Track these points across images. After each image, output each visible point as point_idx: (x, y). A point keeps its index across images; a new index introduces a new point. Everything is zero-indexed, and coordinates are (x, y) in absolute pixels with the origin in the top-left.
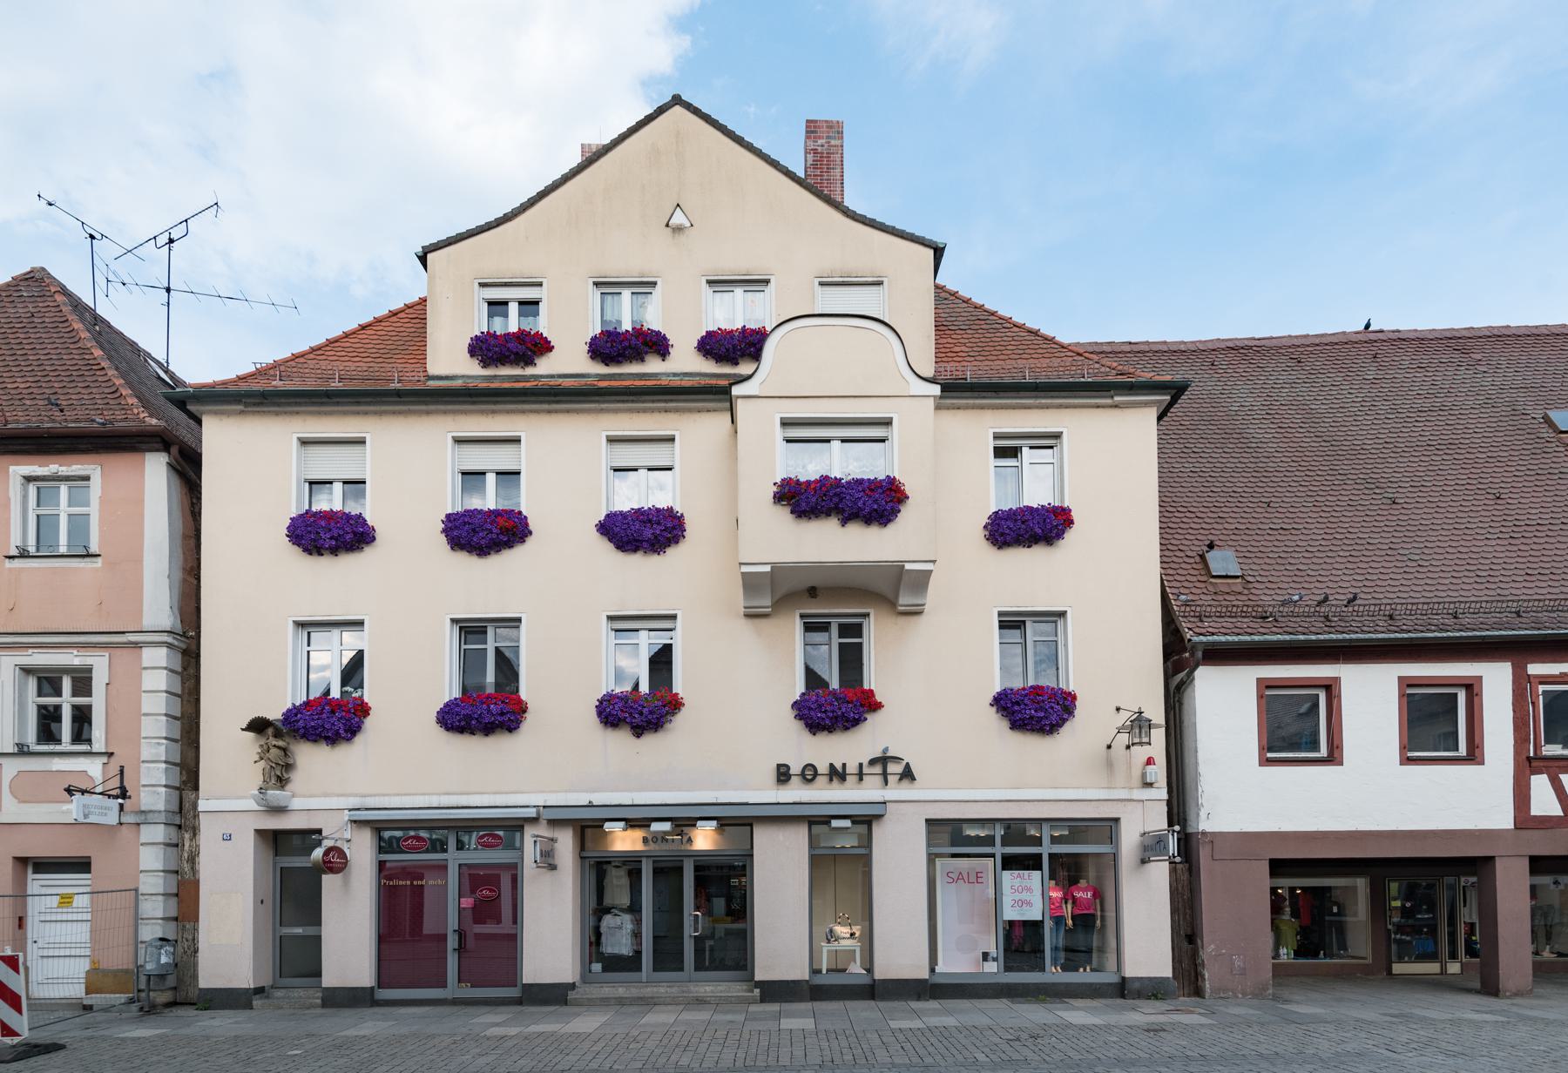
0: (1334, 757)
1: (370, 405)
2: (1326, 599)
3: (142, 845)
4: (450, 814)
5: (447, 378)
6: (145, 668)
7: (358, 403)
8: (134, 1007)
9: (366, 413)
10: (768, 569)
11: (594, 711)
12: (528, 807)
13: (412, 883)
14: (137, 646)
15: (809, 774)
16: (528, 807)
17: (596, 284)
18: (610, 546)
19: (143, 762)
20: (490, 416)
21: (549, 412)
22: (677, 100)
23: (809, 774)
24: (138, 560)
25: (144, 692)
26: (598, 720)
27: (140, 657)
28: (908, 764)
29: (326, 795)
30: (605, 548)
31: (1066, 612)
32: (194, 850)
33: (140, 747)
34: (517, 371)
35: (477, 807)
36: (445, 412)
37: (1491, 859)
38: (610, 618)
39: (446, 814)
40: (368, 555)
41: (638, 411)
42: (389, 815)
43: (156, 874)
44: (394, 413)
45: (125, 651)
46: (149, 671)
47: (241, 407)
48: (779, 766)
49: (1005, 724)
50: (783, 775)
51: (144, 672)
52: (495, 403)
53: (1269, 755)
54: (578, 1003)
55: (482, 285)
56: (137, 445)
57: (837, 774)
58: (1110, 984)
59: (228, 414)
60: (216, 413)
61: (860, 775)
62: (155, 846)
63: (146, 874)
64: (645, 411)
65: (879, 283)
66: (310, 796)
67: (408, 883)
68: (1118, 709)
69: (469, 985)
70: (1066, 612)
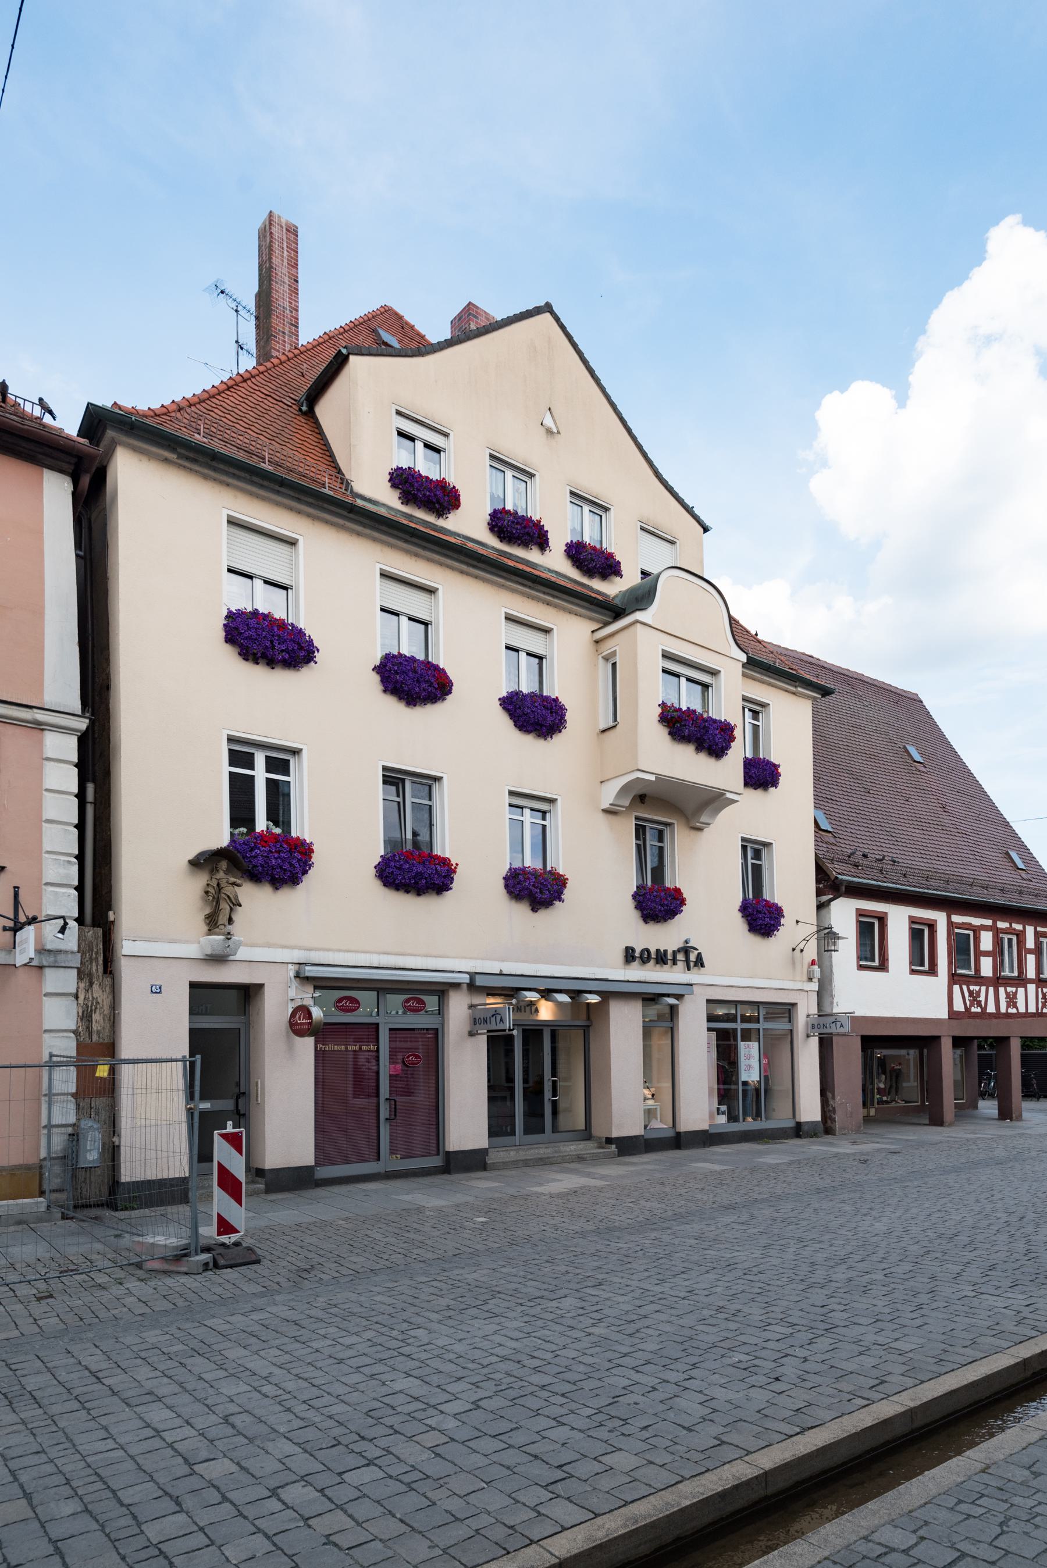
0: (937, 976)
1: (310, 506)
2: (883, 859)
3: (45, 995)
4: (399, 975)
5: (369, 500)
6: (48, 759)
7: (299, 500)
8: (57, 1213)
9: (299, 512)
10: (652, 778)
11: (630, 904)
12: (453, 972)
13: (346, 1049)
14: (39, 727)
15: (645, 957)
16: (453, 972)
17: (492, 456)
18: (511, 723)
19: (47, 884)
20: (414, 558)
21: (462, 572)
22: (548, 308)
23: (645, 957)
24: (39, 612)
25: (47, 790)
26: (505, 891)
27: (41, 743)
28: (699, 954)
29: (269, 945)
30: (503, 722)
31: (442, 778)
32: (90, 1004)
33: (41, 864)
34: (430, 518)
35: (412, 969)
36: (375, 540)
37: (939, 1038)
38: (512, 793)
39: (415, 976)
40: (305, 676)
41: (529, 596)
42: (372, 974)
43: (66, 1034)
44: (327, 522)
45: (18, 731)
46: (52, 763)
47: (172, 456)
48: (627, 948)
49: (746, 927)
50: (629, 956)
51: (49, 765)
52: (424, 548)
53: (861, 963)
54: (496, 1167)
55: (398, 413)
56: (40, 456)
57: (661, 958)
58: (788, 1128)
59: (151, 456)
60: (135, 449)
61: (675, 962)
62: (64, 998)
63: (53, 1034)
64: (533, 598)
65: (672, 543)
66: (252, 946)
67: (343, 1048)
68: (797, 922)
69: (399, 1156)
70: (442, 778)
